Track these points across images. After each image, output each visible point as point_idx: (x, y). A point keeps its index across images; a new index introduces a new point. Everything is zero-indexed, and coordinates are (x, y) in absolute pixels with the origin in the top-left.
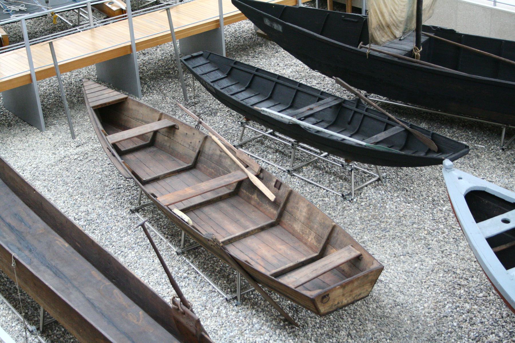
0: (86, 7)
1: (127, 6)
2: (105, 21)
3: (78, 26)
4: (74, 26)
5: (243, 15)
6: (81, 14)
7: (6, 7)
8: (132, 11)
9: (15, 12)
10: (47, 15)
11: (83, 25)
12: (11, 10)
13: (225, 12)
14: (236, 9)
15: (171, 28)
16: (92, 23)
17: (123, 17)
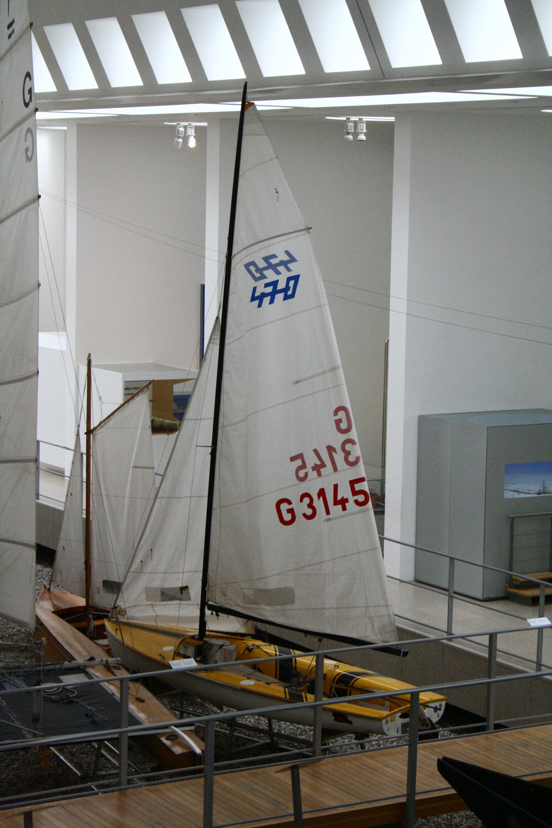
1: (206, 747)
3: (93, 779)
4: (85, 778)
5: (461, 800)
6: (103, 752)
8: (216, 760)
13: (420, 787)
14: (445, 784)
15: (295, 810)
16: (124, 777)
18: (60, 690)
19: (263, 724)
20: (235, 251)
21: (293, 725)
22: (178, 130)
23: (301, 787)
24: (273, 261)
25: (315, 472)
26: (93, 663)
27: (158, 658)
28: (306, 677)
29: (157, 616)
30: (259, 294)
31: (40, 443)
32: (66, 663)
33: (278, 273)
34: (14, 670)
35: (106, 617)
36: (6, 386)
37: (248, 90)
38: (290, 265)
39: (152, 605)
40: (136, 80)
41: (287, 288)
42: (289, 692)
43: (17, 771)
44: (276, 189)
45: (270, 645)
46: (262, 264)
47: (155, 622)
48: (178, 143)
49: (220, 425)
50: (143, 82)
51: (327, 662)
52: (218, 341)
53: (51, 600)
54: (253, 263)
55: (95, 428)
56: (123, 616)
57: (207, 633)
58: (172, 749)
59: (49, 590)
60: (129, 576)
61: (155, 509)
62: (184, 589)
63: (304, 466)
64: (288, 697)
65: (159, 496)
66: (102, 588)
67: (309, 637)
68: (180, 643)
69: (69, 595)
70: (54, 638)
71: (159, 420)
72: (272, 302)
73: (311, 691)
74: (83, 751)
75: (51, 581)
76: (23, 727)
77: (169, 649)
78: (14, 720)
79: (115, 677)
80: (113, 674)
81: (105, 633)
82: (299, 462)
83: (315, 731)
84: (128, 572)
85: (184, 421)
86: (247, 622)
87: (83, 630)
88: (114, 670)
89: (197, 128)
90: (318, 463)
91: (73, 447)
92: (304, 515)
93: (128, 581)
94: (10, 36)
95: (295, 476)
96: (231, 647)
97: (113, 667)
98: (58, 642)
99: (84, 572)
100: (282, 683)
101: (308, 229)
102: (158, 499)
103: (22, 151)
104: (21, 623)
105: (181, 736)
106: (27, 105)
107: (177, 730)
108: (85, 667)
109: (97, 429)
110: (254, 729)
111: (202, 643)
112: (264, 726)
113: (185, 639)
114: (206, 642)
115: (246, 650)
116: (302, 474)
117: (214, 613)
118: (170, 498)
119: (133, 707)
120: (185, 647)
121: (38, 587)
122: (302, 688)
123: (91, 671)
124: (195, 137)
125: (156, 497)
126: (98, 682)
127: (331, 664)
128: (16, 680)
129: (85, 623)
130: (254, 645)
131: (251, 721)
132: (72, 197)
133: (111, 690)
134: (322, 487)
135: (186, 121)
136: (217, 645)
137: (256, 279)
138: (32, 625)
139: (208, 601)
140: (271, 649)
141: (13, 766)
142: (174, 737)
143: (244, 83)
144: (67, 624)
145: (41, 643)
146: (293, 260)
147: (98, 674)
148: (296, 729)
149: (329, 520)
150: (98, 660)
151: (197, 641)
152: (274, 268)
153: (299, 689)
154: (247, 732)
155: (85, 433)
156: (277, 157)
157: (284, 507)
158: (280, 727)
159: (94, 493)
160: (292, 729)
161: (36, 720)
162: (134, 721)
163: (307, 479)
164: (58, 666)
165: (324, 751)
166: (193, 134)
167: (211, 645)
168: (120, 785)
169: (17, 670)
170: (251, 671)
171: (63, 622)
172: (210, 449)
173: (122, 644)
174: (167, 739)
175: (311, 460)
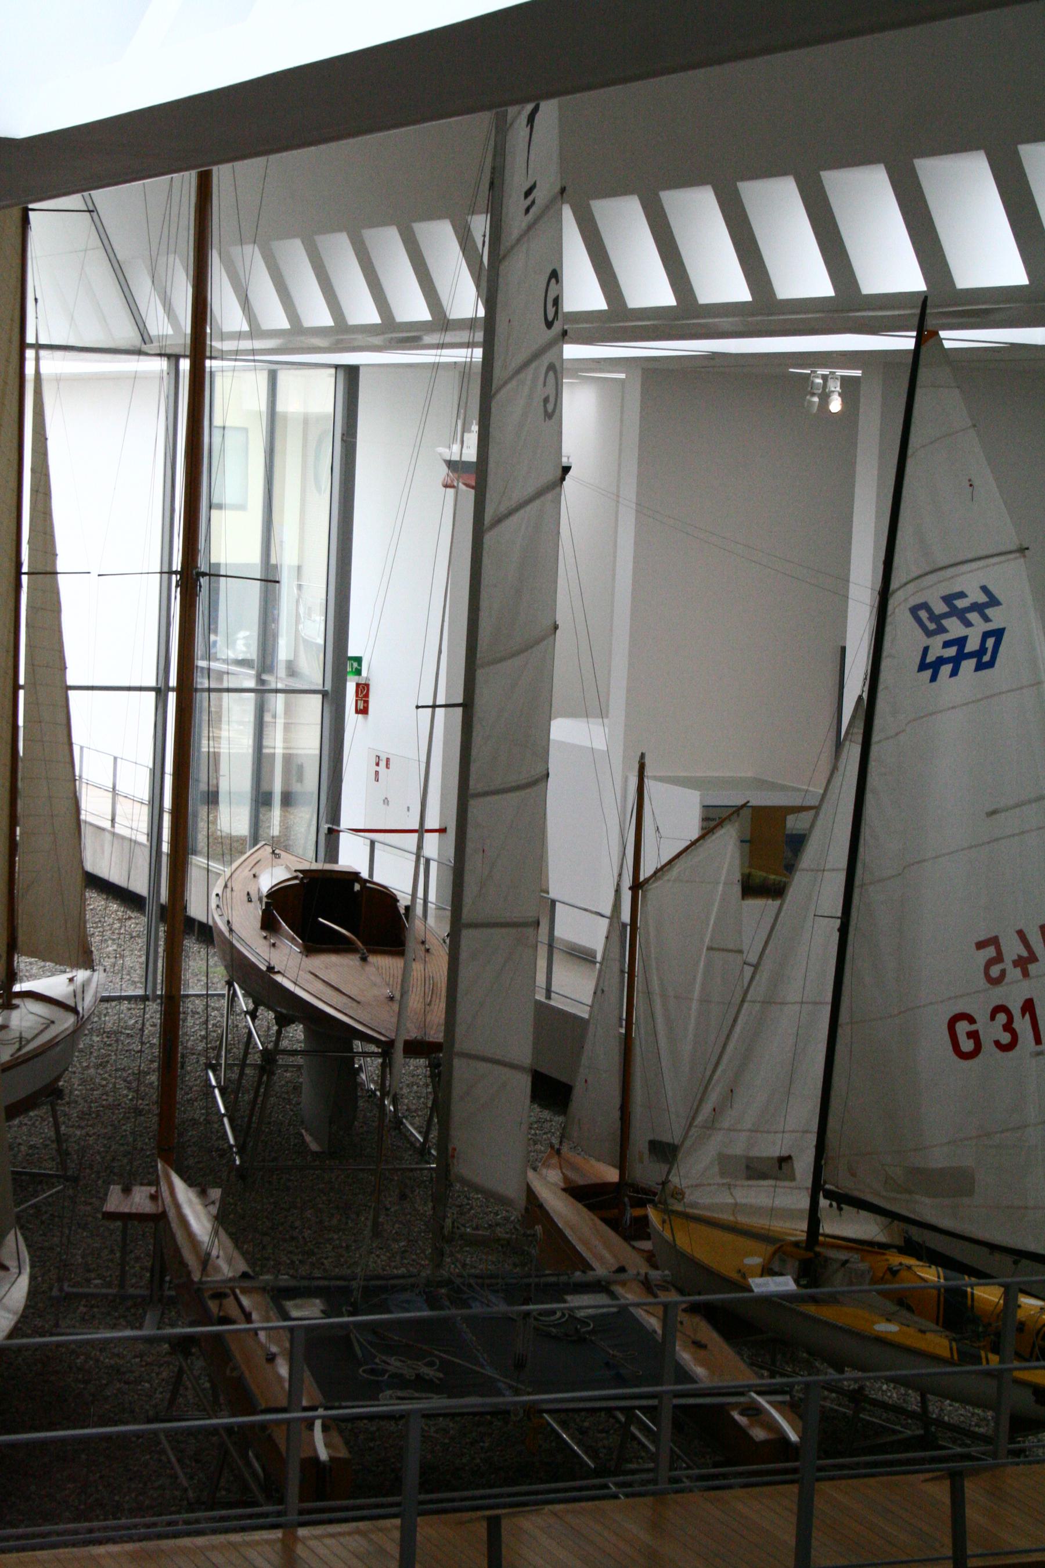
0: (654, 1408)
2: (715, 1477)
3: (615, 1474)
4: (598, 1473)
6: (633, 1429)
7: (375, 1357)
9: (399, 1382)
10: (508, 1412)
11: (633, 1472)
12: (384, 1371)
17: (786, 1471)
18: (564, 1320)
19: (913, 1401)
20: (894, 585)
21: (965, 1408)
22: (813, 382)
23: (967, 1511)
24: (961, 604)
25: (1018, 970)
26: (622, 1276)
27: (734, 1275)
28: (990, 1325)
29: (736, 1204)
30: (934, 659)
31: (557, 903)
32: (578, 1273)
33: (968, 624)
34: (488, 1281)
35: (651, 1201)
36: (496, 797)
37: (928, 311)
38: (989, 612)
39: (729, 1185)
40: (740, 292)
41: (983, 650)
42: (957, 1349)
43: (488, 1454)
44: (970, 480)
45: (930, 1267)
46: (940, 608)
47: (733, 1214)
48: (811, 403)
49: (857, 882)
50: (752, 294)
51: (1026, 1301)
52: (859, 738)
53: (561, 1168)
54: (925, 606)
55: (647, 880)
56: (680, 1200)
57: (821, 1238)
58: (751, 1433)
59: (558, 1152)
60: (690, 1134)
61: (740, 1021)
62: (785, 1160)
63: (999, 958)
64: (956, 1357)
65: (749, 998)
66: (646, 1151)
67: (998, 1256)
68: (774, 1253)
69: (593, 1162)
70: (560, 1232)
71: (759, 875)
72: (954, 673)
73: (996, 1349)
74: (601, 1428)
75: (562, 1137)
76: (497, 1376)
77: (755, 1261)
78: (485, 1363)
79: (651, 1300)
80: (656, 1296)
81: (649, 1230)
82: (990, 952)
83: (997, 1420)
84: (691, 1125)
85: (796, 871)
86: (890, 1223)
87: (614, 1224)
88: (658, 1292)
89: (844, 379)
90: (1025, 954)
91: (607, 911)
92: (997, 1044)
93: (688, 1143)
94: (527, 211)
95: (982, 975)
96: (860, 1263)
97: (656, 1285)
98: (566, 1238)
99: (618, 1123)
100: (947, 1333)
101: (1022, 550)
102: (746, 1005)
103: (538, 400)
104: (503, 1201)
105: (766, 1409)
106: (549, 325)
107: (761, 1400)
108: (609, 1283)
109: (651, 881)
110: (898, 1410)
111: (811, 1255)
112: (914, 1407)
113: (782, 1246)
114: (818, 1255)
115: (888, 1272)
116: (995, 971)
117: (834, 1204)
118: (767, 1002)
119: (685, 1356)
120: (783, 1261)
121: (543, 1148)
122: (982, 1344)
123: (618, 1289)
124: (840, 395)
125: (743, 1001)
126: (627, 1305)
127: (1033, 1305)
128: (492, 1298)
129: (616, 1211)
130: (901, 1264)
131: (891, 1394)
132: (630, 492)
133: (651, 1325)
134: (1028, 997)
135: (826, 367)
136: (836, 1260)
137: (929, 634)
138: (521, 1201)
139: (825, 1183)
140: (931, 1274)
141: (481, 1444)
142: (753, 1411)
143: (922, 299)
144: (585, 1210)
145: (534, 1235)
146: (994, 601)
147: (630, 1295)
148: (969, 1415)
149: (1039, 1054)
150: (632, 1271)
151: (802, 1252)
152: (960, 615)
153: (975, 1345)
154: (885, 1415)
155: (630, 888)
156: (974, 426)
157: (962, 1027)
158: (942, 1410)
159: (640, 988)
160: (962, 1415)
161: (520, 1365)
162: (684, 1375)
163: (1004, 983)
164: (563, 1279)
165: (1017, 1453)
166: (838, 389)
167: (827, 1260)
168: (656, 1484)
169: (493, 1281)
170: (894, 1308)
171: (580, 1206)
172: (838, 923)
173: (673, 1246)
174: (742, 1414)
175: (1013, 949)
